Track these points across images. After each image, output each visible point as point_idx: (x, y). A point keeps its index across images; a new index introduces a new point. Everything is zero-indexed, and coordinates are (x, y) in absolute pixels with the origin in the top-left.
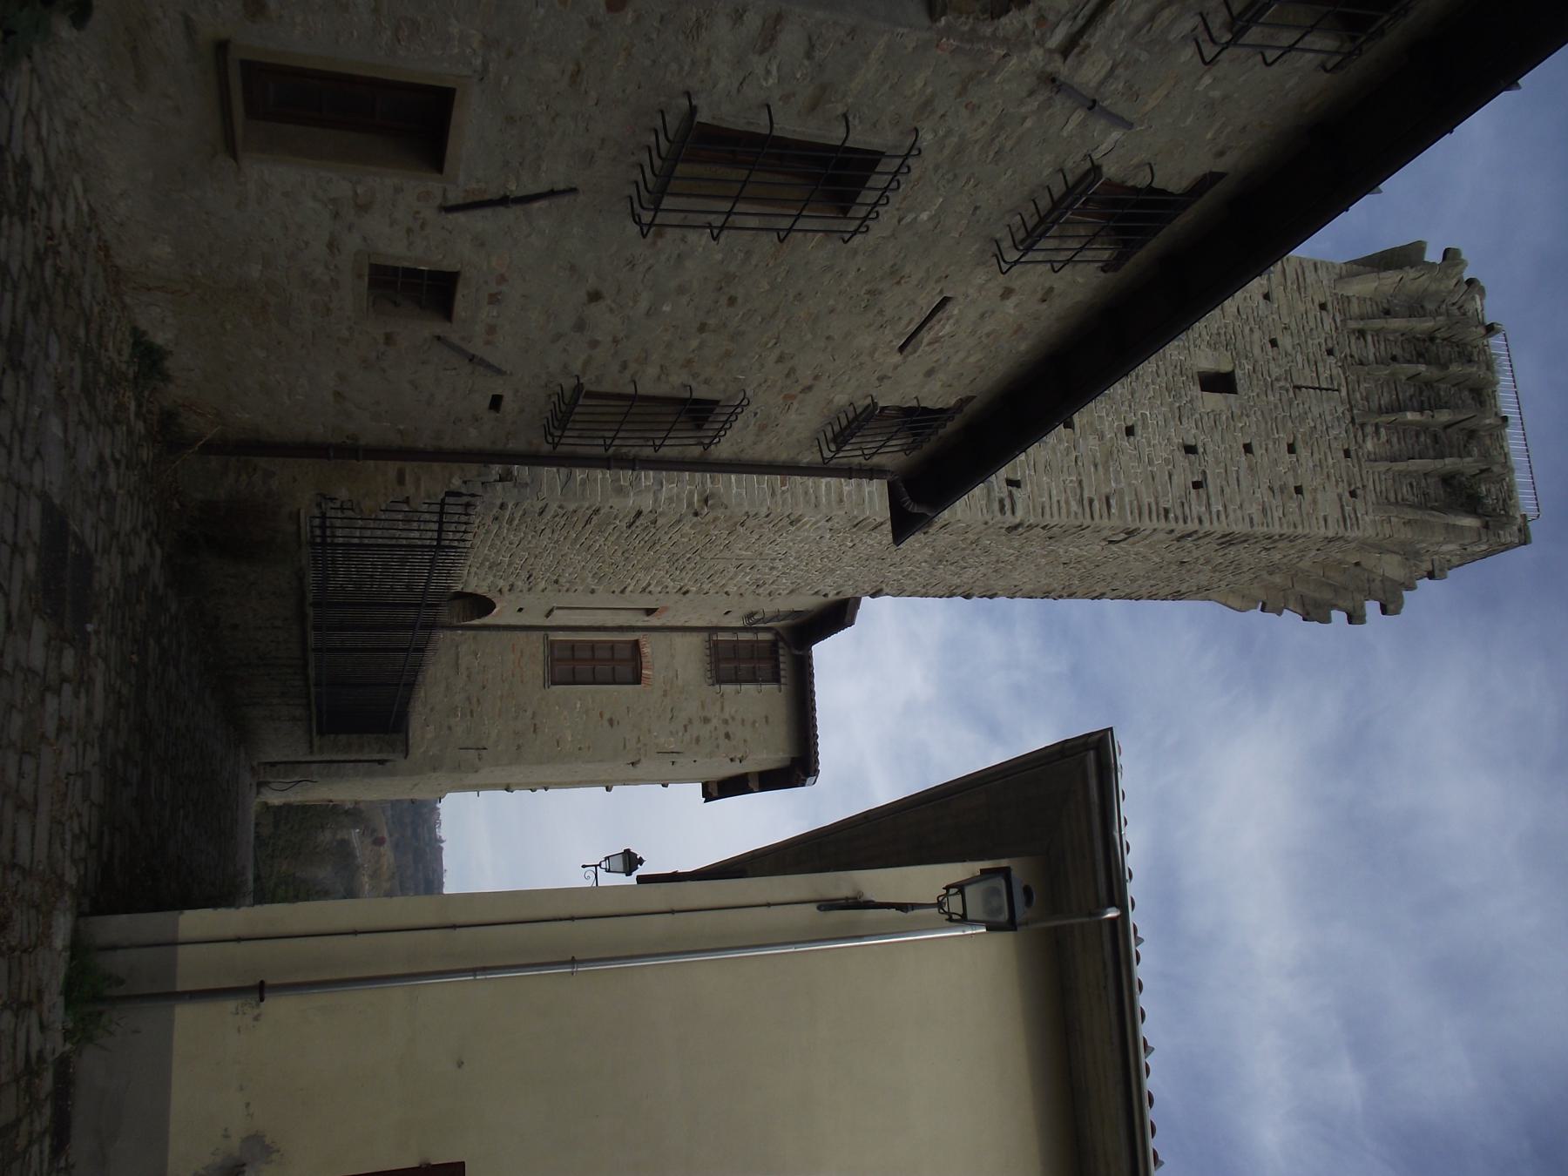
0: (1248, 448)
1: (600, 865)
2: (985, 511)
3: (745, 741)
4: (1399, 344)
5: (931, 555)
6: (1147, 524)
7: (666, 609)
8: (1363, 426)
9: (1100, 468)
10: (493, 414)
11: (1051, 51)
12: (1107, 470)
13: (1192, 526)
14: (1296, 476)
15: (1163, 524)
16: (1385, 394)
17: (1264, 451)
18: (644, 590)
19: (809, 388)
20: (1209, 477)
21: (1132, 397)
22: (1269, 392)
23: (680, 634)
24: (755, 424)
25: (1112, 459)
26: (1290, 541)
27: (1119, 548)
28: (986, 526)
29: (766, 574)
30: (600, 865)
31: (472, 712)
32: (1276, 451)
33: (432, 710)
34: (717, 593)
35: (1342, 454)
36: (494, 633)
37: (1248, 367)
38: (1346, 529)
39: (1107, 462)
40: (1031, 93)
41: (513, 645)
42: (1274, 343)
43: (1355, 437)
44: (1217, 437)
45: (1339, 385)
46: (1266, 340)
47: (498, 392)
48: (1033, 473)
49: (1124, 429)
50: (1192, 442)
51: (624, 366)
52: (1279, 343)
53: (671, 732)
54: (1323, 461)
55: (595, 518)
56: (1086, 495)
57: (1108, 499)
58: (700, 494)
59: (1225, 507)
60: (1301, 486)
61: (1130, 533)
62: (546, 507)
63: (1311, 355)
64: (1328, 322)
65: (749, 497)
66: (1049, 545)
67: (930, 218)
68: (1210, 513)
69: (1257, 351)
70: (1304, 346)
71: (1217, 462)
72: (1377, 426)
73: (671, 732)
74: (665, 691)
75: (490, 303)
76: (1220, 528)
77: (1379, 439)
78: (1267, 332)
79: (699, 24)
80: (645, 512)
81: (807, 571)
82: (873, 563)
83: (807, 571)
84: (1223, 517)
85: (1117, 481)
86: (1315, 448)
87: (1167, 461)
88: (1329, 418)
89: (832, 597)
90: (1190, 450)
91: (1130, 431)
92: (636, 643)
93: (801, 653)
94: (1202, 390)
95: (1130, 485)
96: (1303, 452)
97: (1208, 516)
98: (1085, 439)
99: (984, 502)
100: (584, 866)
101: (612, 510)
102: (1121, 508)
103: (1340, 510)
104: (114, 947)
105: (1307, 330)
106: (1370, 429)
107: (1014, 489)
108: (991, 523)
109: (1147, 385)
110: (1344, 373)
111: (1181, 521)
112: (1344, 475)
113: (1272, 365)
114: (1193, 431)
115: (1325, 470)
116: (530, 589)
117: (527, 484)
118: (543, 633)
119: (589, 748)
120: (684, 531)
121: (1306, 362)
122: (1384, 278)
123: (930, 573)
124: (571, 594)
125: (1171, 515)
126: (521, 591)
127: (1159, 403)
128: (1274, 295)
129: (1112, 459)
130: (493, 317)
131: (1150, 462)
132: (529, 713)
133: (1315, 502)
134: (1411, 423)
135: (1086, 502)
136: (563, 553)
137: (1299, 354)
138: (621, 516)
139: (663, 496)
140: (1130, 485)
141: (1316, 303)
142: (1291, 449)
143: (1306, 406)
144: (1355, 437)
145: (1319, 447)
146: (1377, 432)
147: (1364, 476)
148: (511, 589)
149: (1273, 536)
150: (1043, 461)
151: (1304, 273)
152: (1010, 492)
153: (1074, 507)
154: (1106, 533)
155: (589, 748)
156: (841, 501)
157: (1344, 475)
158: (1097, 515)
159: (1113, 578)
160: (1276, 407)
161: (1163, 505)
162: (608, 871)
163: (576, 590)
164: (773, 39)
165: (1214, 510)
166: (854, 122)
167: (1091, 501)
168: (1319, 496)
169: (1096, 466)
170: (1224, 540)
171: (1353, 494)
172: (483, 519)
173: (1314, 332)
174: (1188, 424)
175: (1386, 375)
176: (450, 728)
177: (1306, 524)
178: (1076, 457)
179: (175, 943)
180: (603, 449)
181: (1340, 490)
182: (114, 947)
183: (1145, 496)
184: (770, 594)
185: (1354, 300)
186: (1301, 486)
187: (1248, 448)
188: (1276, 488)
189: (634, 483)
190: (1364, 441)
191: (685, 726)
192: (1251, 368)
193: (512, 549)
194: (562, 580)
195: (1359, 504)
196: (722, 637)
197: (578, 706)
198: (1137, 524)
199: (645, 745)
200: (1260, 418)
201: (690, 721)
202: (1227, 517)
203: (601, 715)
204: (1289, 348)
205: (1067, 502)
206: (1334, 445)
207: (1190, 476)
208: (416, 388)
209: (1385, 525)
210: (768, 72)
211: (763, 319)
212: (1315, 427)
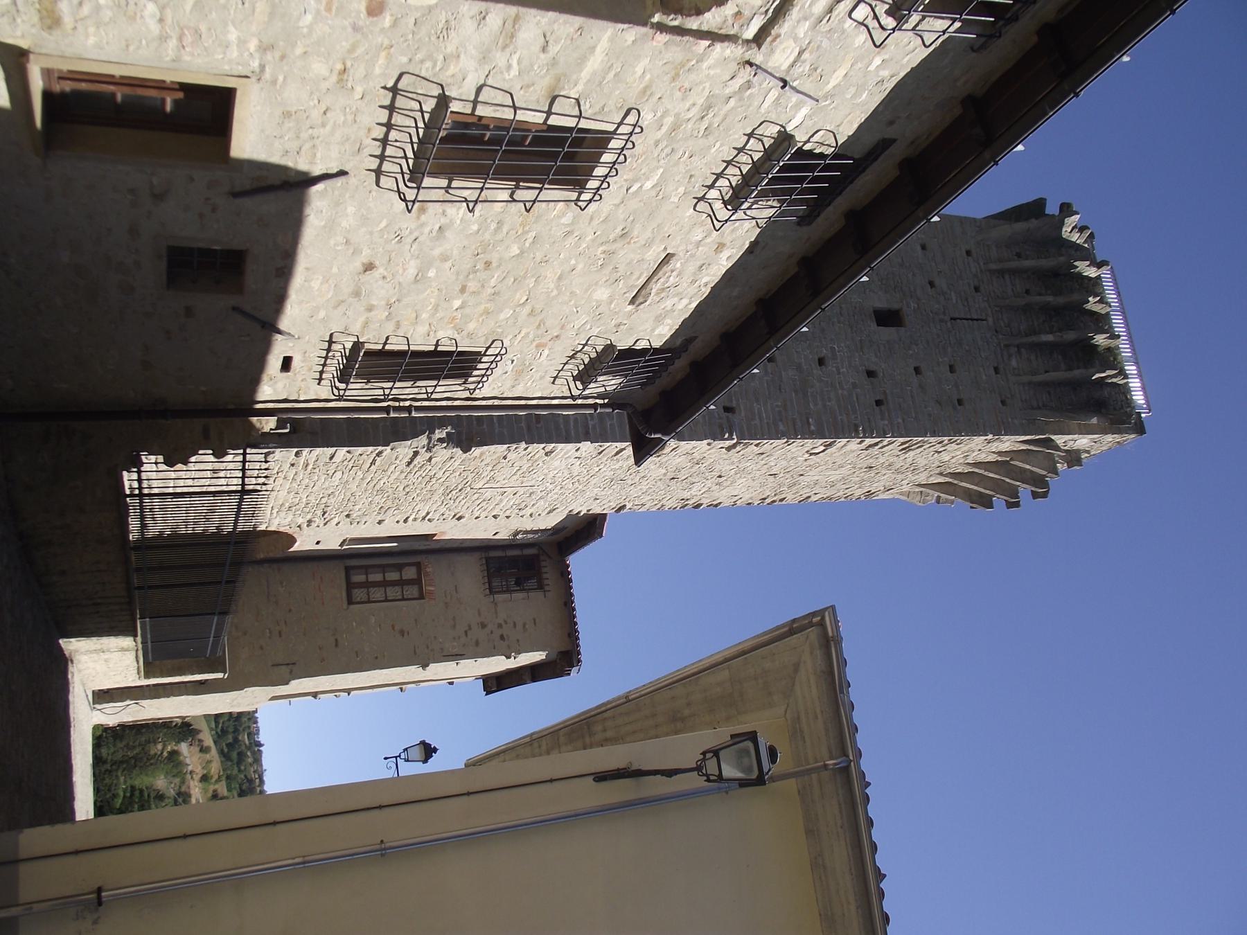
1: (399, 756)
30: (399, 756)
42: (932, 284)
47: (285, 374)
100: (386, 758)
170: (904, 446)
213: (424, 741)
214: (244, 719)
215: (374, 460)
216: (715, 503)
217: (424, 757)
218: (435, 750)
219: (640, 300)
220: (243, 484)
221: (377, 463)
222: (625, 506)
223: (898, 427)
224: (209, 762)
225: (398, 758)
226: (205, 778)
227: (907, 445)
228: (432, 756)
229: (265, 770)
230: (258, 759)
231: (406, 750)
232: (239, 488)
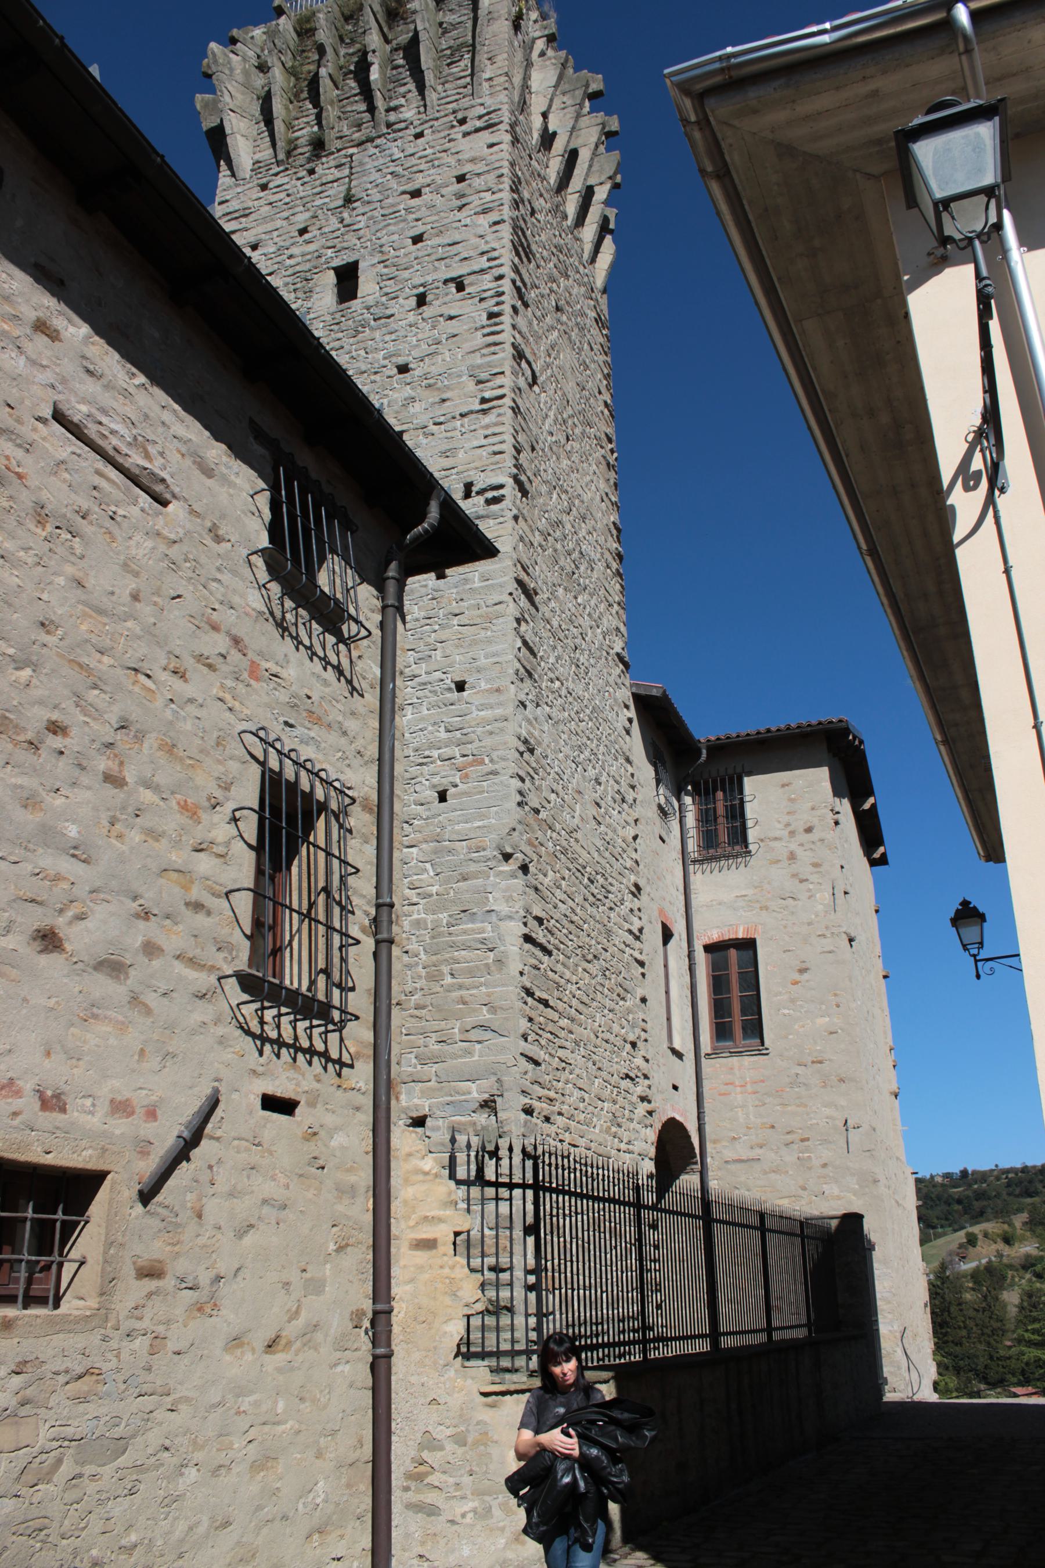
0: (417, 239)
1: (974, 956)
2: (501, 520)
3: (813, 809)
4: (301, 104)
5: (565, 589)
7: (661, 911)
8: (389, 125)
12: (448, 388)
13: (506, 285)
15: (507, 319)
16: (354, 108)
17: (420, 223)
18: (637, 938)
19: (236, 641)
20: (449, 276)
21: (365, 372)
22: (355, 227)
23: (693, 896)
24: (309, 729)
25: (435, 384)
26: (520, 183)
27: (541, 374)
28: (520, 519)
29: (605, 790)
30: (974, 956)
31: (803, 1140)
32: (419, 210)
33: (804, 1188)
34: (636, 850)
36: (706, 1119)
37: (329, 253)
38: (502, 122)
39: (439, 389)
41: (720, 1095)
42: (303, 231)
43: (400, 130)
44: (406, 274)
45: (346, 156)
46: (300, 240)
47: (258, 1103)
48: (454, 471)
49: (401, 376)
50: (413, 302)
51: (197, 906)
52: (302, 226)
53: (810, 897)
54: (428, 159)
56: (478, 407)
59: (483, 253)
60: (456, 177)
61: (519, 355)
62: (526, 1056)
63: (315, 191)
64: (279, 180)
65: (500, 803)
66: (543, 450)
68: (490, 268)
69: (312, 247)
70: (305, 200)
71: (436, 269)
72: (388, 111)
73: (810, 897)
74: (761, 908)
75: (63, 1110)
76: (507, 256)
77: (402, 106)
78: (292, 241)
80: (526, 931)
81: (599, 740)
82: (582, 660)
83: (599, 740)
86: (415, 169)
89: (632, 713)
90: (422, 301)
91: (403, 369)
92: (708, 948)
93: (704, 752)
94: (355, 297)
96: (419, 181)
97: (494, 270)
100: (978, 977)
101: (525, 972)
103: (480, 134)
105: (288, 200)
106: (392, 117)
107: (475, 489)
108: (515, 511)
109: (352, 358)
110: (333, 153)
111: (502, 298)
112: (442, 134)
113: (326, 230)
115: (438, 155)
116: (646, 1077)
117: (499, 1081)
118: (703, 1059)
119: (836, 995)
120: (551, 884)
121: (322, 195)
122: (232, 128)
123: (591, 595)
124: (648, 1027)
125: (496, 309)
126: (649, 1087)
127: (370, 343)
129: (435, 384)
130: (94, 1105)
132: (800, 1070)
133: (472, 160)
134: (382, 72)
135: (485, 406)
136: (592, 1036)
137: (314, 204)
138: (534, 962)
139: (503, 908)
141: (262, 194)
142: (416, 194)
143: (369, 186)
144: (400, 130)
145: (412, 166)
146: (395, 109)
147: (442, 114)
148: (643, 1099)
149: (515, 200)
150: (441, 460)
151: (230, 213)
152: (478, 493)
153: (487, 419)
154: (522, 383)
155: (836, 995)
156: (498, 690)
157: (442, 134)
158: (499, 392)
159: (584, 389)
160: (370, 219)
161: (485, 322)
162: (981, 943)
163: (643, 1020)
165: (488, 264)
167: (484, 401)
169: (444, 401)
170: (522, 253)
171: (463, 122)
172: (548, 1135)
173: (290, 192)
174: (394, 308)
175: (333, 110)
176: (825, 1165)
177: (497, 165)
178: (435, 424)
181: (460, 136)
183: (475, 343)
184: (633, 787)
185: (257, 157)
186: (456, 177)
187: (417, 239)
188: (459, 203)
189: (490, 946)
190: (405, 121)
191: (802, 881)
192: (330, 251)
193: (590, 1098)
194: (631, 1037)
196: (692, 845)
197: (786, 1011)
199: (827, 928)
200: (384, 232)
201: (794, 876)
202: (495, 250)
203: (795, 983)
205: (487, 427)
207: (451, 296)
208: (251, 1226)
209: (495, 83)
211: (95, 687)
212: (391, 174)
213: (951, 919)
214: (922, 1186)
215: (540, 1001)
216: (615, 532)
217: (975, 919)
218: (965, 903)
219: (159, 488)
220: (524, 1186)
221: (545, 996)
222: (618, 654)
223: (495, 259)
224: (986, 1235)
225: (978, 958)
226: (1008, 1240)
227: (520, 249)
228: (975, 907)
229: (997, 1166)
230: (982, 1176)
231: (965, 947)
232: (530, 1193)
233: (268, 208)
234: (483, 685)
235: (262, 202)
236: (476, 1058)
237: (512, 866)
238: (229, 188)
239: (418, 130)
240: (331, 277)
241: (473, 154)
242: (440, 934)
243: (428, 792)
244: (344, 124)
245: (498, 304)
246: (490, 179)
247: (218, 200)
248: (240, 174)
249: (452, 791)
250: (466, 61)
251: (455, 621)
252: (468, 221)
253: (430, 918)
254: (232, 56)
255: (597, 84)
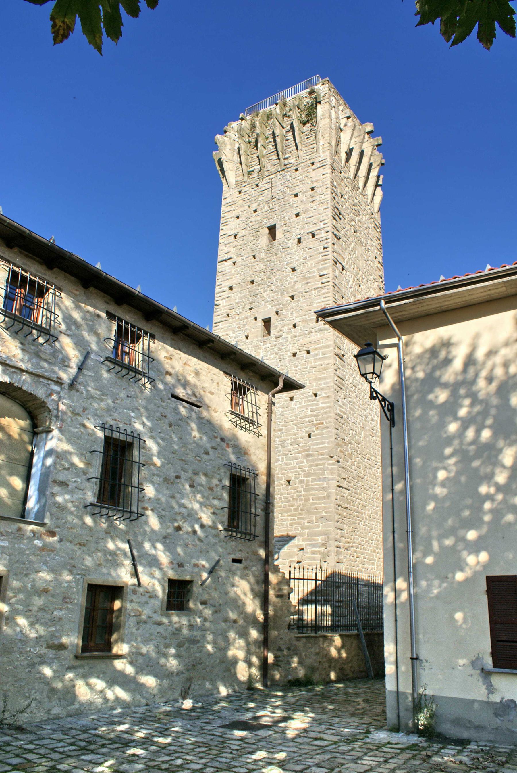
0: (297, 215)
6: (330, 257)
9: (308, 281)
10: (243, 562)
11: (61, 389)
14: (307, 192)
15: (330, 249)
35: (297, 172)
39: (306, 278)
40: (77, 391)
42: (255, 211)
55: (343, 506)
56: (320, 285)
57: (321, 276)
58: (329, 460)
67: (133, 412)
69: (258, 218)
72: (285, 159)
79: (58, 507)
84: (325, 222)
85: (314, 272)
87: (304, 251)
88: (283, 181)
90: (299, 241)
95: (315, 267)
96: (297, 190)
98: (297, 289)
99: (326, 332)
102: (324, 269)
104: (398, 716)
105: (249, 197)
106: (286, 162)
113: (264, 210)
114: (292, 241)
125: (326, 246)
128: (237, 215)
131: (305, 258)
133: (316, 181)
135: (323, 285)
140: (315, 267)
142: (296, 195)
153: (324, 291)
154: (337, 273)
156: (328, 397)
161: (322, 250)
164: (62, 482)
166: (93, 449)
167: (322, 283)
168: (314, 179)
174: (289, 244)
179: (398, 692)
180: (257, 518)
181: (311, 170)
182: (398, 716)
187: (297, 215)
188: (312, 200)
195: (316, 161)
198: (331, 260)
204: (257, 204)
205: (324, 294)
206: (293, 176)
210: (75, 481)
233: (241, 201)
234: (324, 395)
235: (240, 198)
236: (320, 528)
237: (332, 461)
238: (227, 192)
239: (296, 167)
240: (267, 231)
241: (316, 178)
242: (309, 485)
243: (304, 434)
244: (269, 165)
245: (327, 243)
246: (323, 188)
247: (223, 197)
248: (231, 187)
249: (312, 433)
250: (314, 137)
251: (313, 370)
252: (315, 207)
253: (305, 479)
254: (225, 138)
255: (369, 127)
